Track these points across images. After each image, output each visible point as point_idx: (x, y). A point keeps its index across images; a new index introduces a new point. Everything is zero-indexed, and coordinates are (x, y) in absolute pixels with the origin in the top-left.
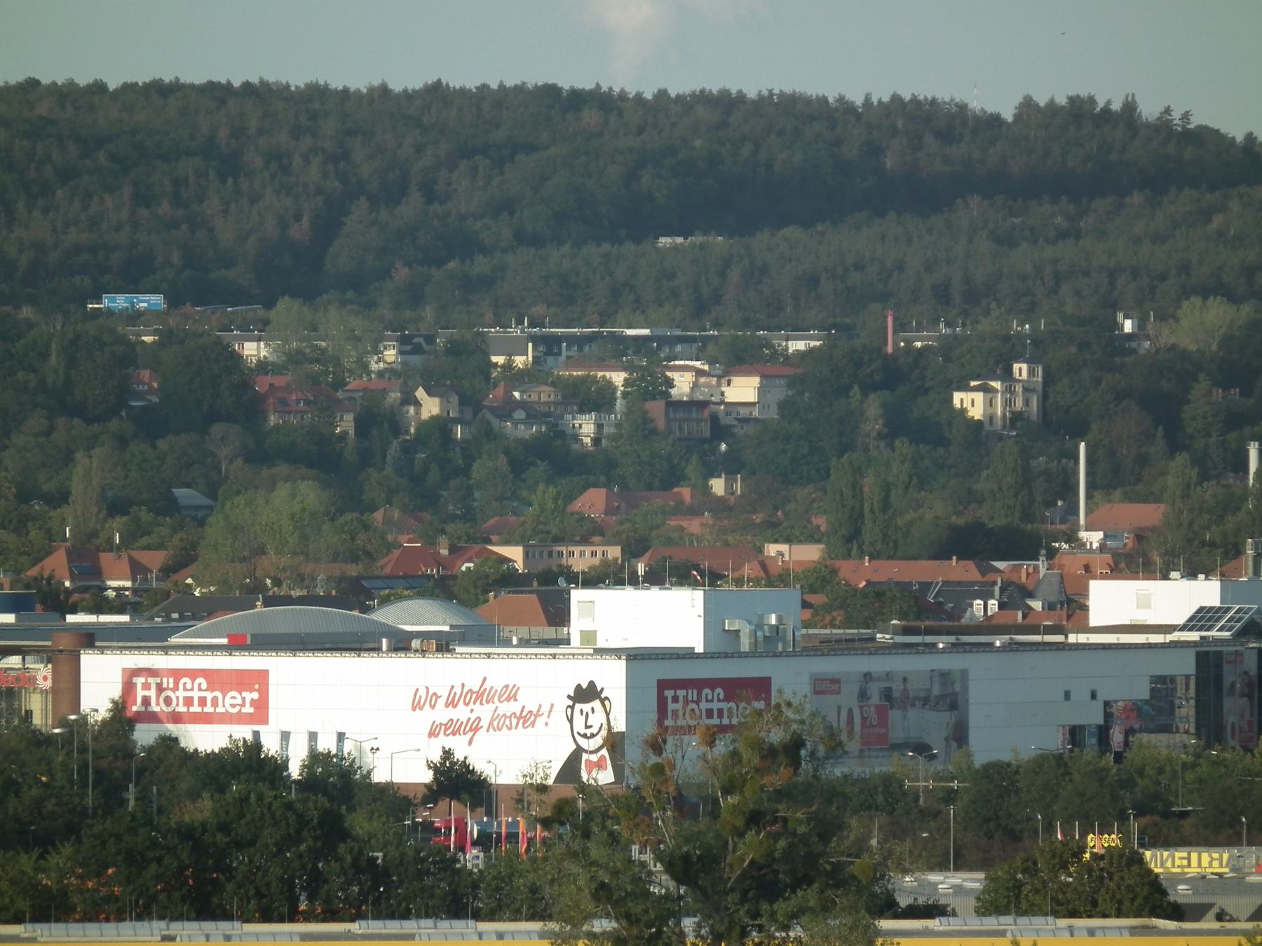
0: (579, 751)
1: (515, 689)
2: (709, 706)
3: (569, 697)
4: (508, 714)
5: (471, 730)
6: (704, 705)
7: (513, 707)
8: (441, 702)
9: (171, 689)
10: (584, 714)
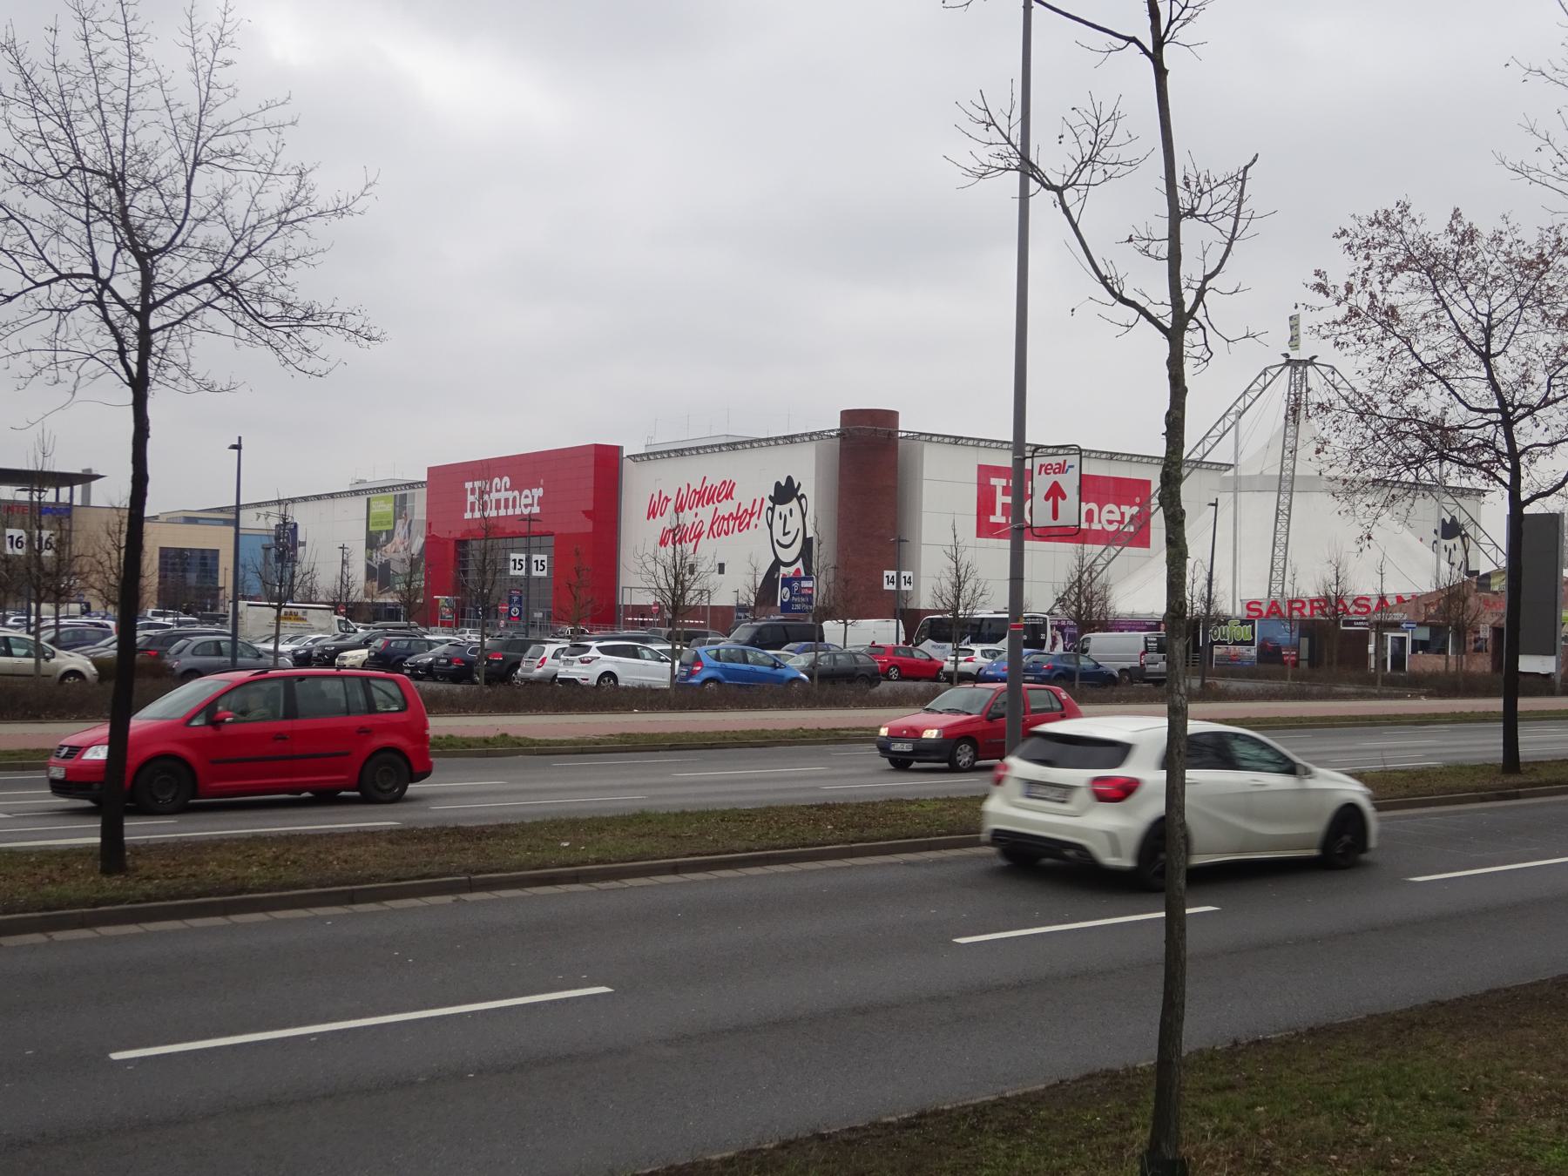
0: (777, 563)
4: (726, 516)
5: (694, 537)
6: (494, 496)
7: (726, 508)
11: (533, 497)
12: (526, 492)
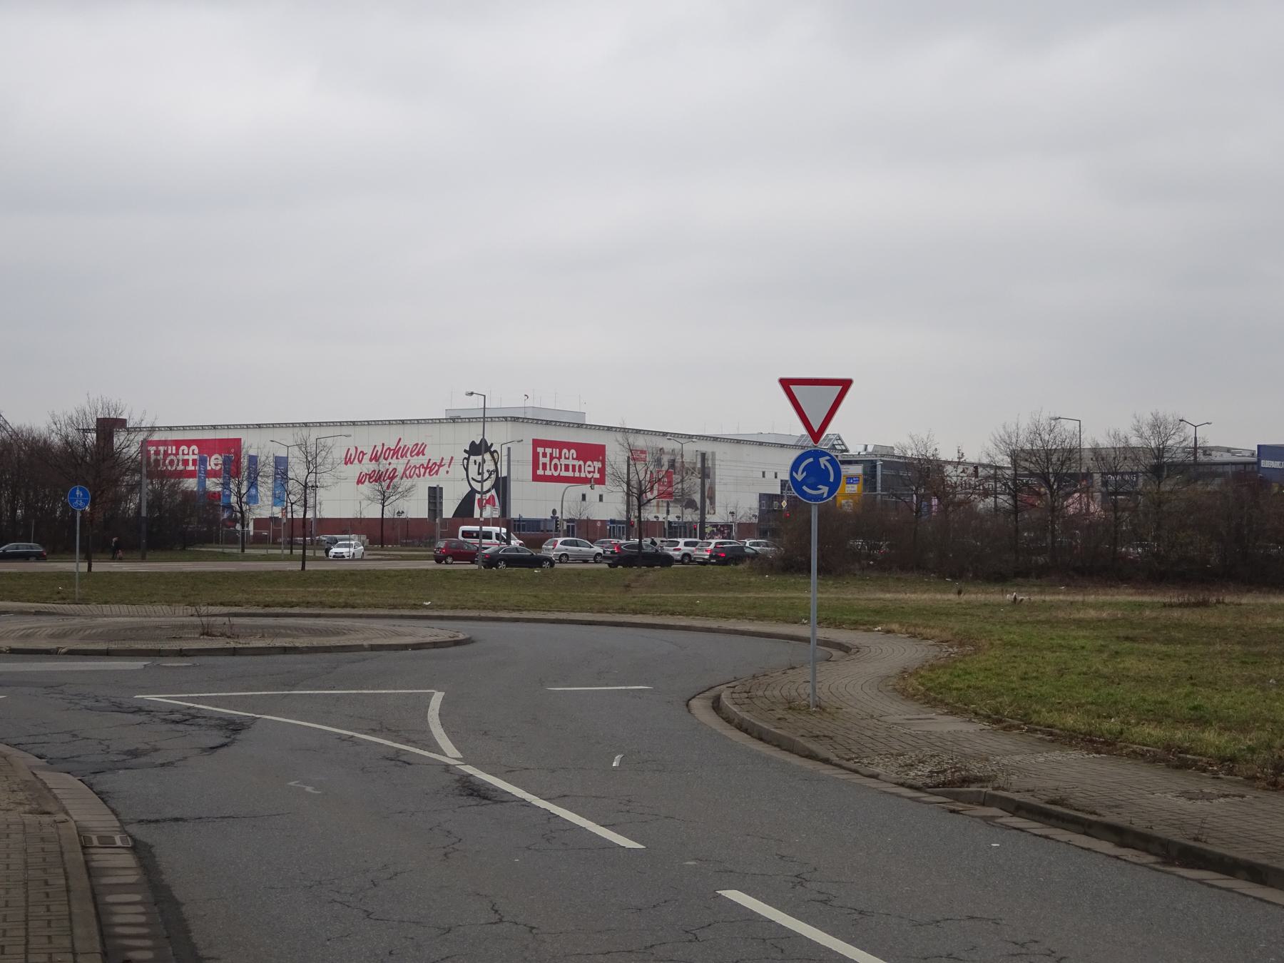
0: (473, 492)
1: (424, 446)
2: (567, 462)
3: (465, 451)
4: (418, 466)
5: (389, 478)
6: (563, 462)
7: (422, 460)
8: (367, 457)
9: (174, 454)
10: (478, 464)
11: (594, 467)
12: (589, 463)
